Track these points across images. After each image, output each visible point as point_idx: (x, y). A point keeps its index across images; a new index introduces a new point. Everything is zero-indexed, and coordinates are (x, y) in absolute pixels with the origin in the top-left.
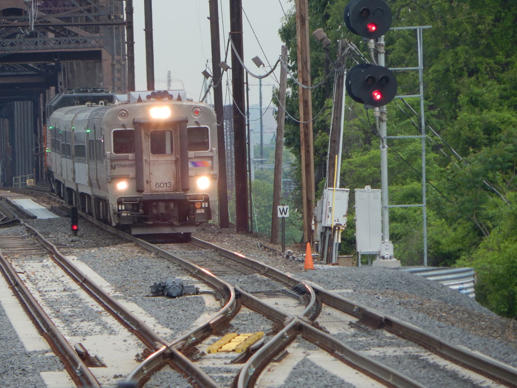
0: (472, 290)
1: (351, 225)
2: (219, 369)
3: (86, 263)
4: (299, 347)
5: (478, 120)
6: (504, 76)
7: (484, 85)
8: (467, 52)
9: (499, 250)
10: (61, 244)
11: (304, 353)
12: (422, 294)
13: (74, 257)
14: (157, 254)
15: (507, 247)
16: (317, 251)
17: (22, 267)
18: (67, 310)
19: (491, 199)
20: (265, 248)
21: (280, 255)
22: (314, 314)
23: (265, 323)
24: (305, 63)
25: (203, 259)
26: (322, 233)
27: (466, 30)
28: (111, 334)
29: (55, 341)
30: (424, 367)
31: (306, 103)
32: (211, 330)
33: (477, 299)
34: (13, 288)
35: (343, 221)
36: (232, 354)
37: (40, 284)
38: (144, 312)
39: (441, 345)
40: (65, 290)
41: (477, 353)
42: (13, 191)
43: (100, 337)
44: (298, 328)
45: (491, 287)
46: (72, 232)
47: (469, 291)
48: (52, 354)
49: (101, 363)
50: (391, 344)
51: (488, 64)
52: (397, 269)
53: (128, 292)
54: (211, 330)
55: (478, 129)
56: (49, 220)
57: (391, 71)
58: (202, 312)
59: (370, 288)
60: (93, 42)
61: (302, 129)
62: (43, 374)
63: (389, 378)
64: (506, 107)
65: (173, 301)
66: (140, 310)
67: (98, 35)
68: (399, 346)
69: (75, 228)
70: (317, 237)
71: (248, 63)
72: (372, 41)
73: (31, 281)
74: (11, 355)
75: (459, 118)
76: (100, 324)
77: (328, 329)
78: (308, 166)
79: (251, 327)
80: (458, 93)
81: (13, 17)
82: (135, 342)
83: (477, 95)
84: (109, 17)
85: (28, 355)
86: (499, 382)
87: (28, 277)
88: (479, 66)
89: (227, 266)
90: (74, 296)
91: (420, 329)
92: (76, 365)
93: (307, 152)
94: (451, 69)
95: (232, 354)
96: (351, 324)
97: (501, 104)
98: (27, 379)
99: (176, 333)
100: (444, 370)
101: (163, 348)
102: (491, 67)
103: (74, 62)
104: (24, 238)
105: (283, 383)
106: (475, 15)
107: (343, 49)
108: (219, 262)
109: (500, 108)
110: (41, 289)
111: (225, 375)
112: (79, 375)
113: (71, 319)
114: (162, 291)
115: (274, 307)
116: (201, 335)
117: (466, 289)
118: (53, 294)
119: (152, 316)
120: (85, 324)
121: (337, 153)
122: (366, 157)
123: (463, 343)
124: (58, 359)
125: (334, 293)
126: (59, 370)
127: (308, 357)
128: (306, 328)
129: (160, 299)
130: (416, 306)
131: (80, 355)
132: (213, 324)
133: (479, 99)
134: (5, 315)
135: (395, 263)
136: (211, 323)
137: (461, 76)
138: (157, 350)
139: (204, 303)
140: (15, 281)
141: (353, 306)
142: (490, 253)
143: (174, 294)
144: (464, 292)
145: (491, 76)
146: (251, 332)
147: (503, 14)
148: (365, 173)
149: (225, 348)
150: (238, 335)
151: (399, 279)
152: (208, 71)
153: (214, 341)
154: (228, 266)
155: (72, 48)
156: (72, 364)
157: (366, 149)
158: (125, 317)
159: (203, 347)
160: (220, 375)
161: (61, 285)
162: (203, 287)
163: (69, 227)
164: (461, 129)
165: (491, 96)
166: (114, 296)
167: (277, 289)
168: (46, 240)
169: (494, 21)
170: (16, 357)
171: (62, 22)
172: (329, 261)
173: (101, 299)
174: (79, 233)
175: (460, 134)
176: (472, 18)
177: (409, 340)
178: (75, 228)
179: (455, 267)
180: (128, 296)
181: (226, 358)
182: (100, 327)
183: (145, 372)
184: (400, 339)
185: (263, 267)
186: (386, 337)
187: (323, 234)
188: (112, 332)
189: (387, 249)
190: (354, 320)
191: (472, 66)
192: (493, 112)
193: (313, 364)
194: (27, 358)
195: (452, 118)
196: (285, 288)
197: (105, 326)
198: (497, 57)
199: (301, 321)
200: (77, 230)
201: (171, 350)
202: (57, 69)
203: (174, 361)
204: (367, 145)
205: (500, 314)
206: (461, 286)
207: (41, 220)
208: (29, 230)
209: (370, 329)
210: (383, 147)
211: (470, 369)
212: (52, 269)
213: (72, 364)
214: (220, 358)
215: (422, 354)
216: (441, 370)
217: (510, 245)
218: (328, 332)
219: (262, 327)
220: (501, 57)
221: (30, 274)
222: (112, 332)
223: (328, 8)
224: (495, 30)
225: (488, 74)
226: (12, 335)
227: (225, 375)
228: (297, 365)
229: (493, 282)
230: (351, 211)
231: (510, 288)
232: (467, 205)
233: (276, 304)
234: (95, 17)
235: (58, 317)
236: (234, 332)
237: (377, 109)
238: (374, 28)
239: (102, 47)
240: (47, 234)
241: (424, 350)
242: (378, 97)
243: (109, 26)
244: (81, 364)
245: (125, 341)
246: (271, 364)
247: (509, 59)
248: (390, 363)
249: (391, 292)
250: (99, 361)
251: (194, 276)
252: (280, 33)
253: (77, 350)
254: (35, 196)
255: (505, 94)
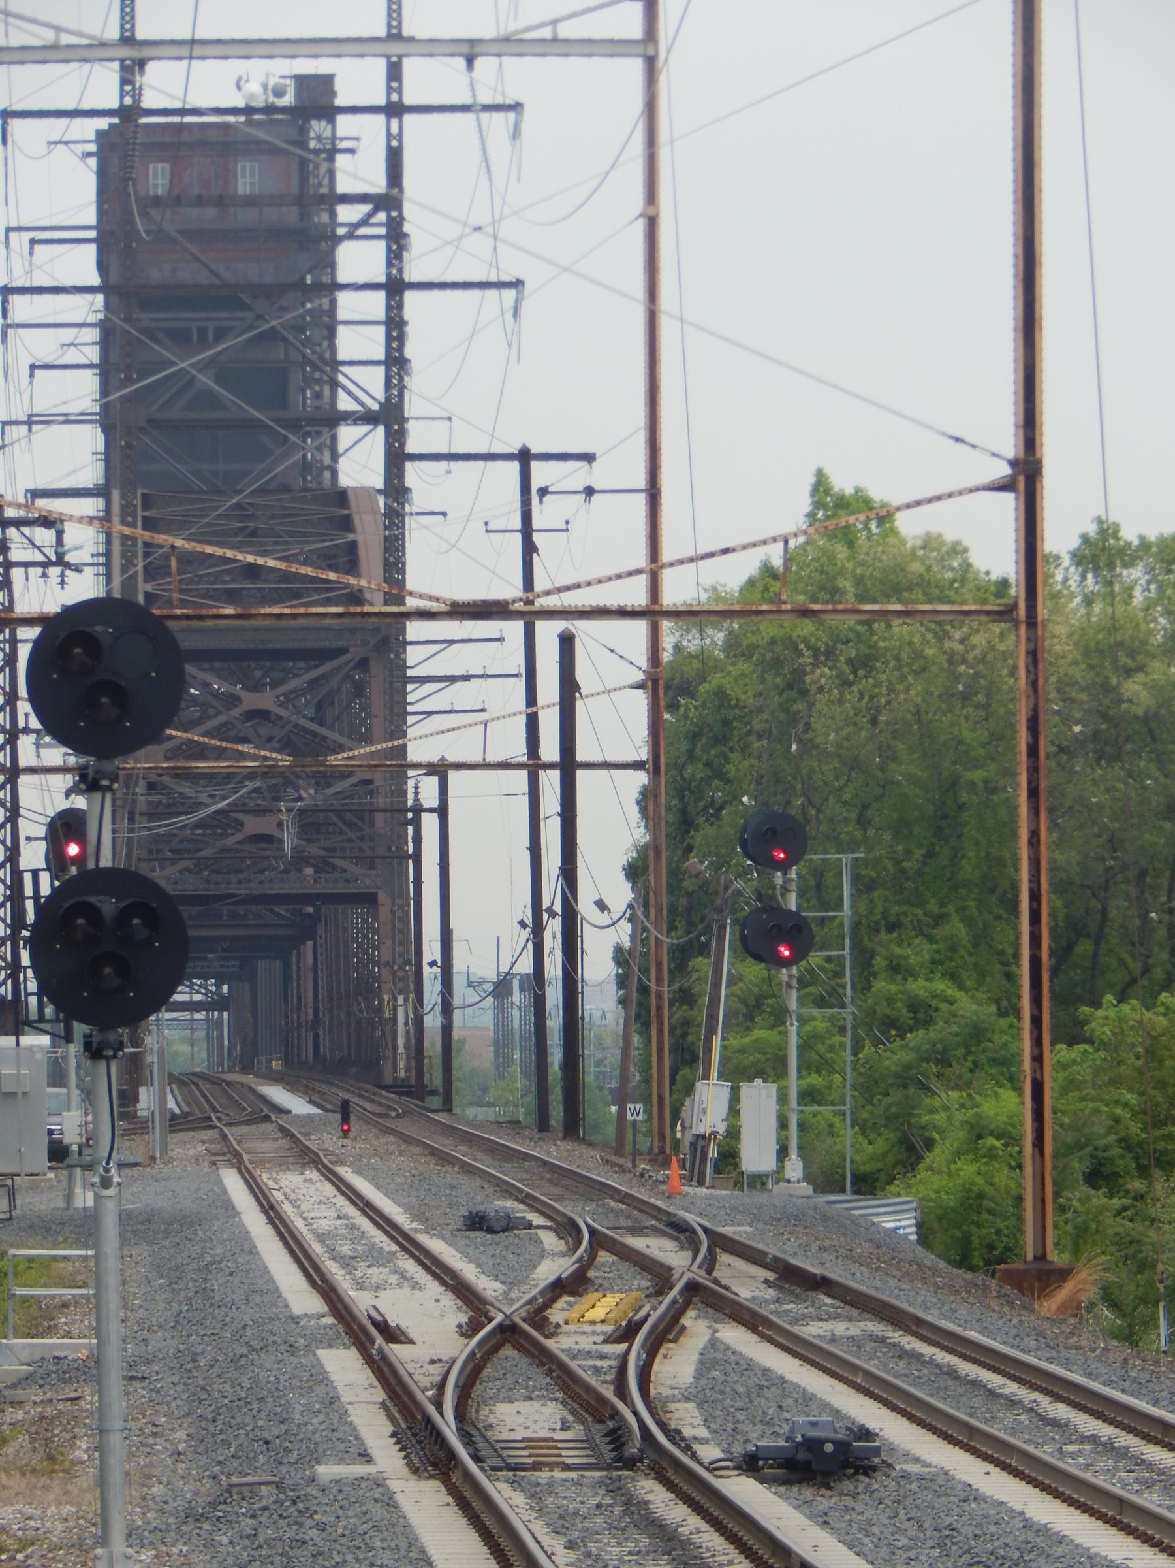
0: (914, 1229)
1: (734, 1133)
2: (589, 1352)
3: (365, 1178)
4: (698, 1317)
5: (900, 992)
6: (937, 932)
7: (909, 945)
8: (886, 899)
9: (950, 1174)
10: (327, 1150)
11: (709, 1327)
12: (845, 1235)
13: (346, 1169)
14: (462, 1167)
15: (960, 1170)
16: (684, 1168)
17: (276, 1181)
18: (346, 1247)
19: (928, 1101)
20: (607, 1161)
21: (630, 1172)
22: (710, 1265)
23: (639, 1277)
24: (659, 910)
25: (528, 1176)
26: (692, 1144)
27: (885, 868)
28: (413, 1288)
29: (335, 1299)
30: (900, 1357)
31: (659, 965)
32: (564, 1287)
33: (919, 1241)
34: (266, 1212)
35: (721, 1128)
36: (600, 1328)
37: (304, 1207)
38: (458, 1255)
39: (919, 1321)
40: (339, 1217)
41: (973, 1335)
42: (257, 1076)
43: (398, 1292)
44: (693, 1288)
45: (936, 1226)
46: (341, 1134)
47: (909, 1230)
48: (329, 1320)
49: (407, 1337)
50: (837, 1317)
51: (915, 915)
52: (808, 1197)
53: (430, 1222)
54: (564, 1287)
55: (899, 1004)
56: (309, 1116)
57: (804, 919)
58: (542, 1256)
59: (771, 1225)
60: (368, 882)
61: (653, 1001)
62: (320, 1352)
63: (857, 1376)
64: (939, 975)
65: (496, 1237)
66: (451, 1251)
67: (373, 872)
68: (850, 1320)
69: (346, 1127)
70: (686, 1147)
71: (585, 906)
72: (779, 874)
73: (291, 1202)
74: (270, 1318)
75: (873, 989)
76: (396, 1272)
77: (734, 1289)
78: (660, 1050)
79: (620, 1282)
80: (873, 955)
81: (263, 845)
82: (452, 1303)
83: (900, 957)
84: (389, 849)
85: (295, 1320)
86: (1030, 1387)
87: (286, 1195)
88: (903, 918)
89: (563, 1187)
90: (353, 1227)
91: (872, 1292)
92: (373, 1342)
93: (660, 1031)
94: (864, 921)
95: (600, 1328)
96: (766, 1281)
97: (932, 972)
98: (295, 1361)
99: (510, 1290)
100: (931, 1362)
101: (499, 1318)
102: (919, 921)
103: (340, 907)
104: (277, 1139)
105: (691, 1380)
106: (900, 848)
107: (726, 888)
108: (551, 1181)
109: (931, 976)
110: (305, 1215)
111: (599, 1363)
112: (377, 1358)
113: (354, 1263)
114: (480, 1223)
115: (647, 1251)
116: (549, 1295)
117: (904, 1227)
118: (323, 1223)
119: (470, 1262)
120: (374, 1271)
121: (716, 1033)
122: (747, 1040)
123: (944, 1316)
124: (341, 1328)
125: (727, 1230)
126: (346, 1347)
127: (717, 1335)
128: (706, 1288)
129: (478, 1236)
130: (842, 1251)
131: (375, 1323)
132: (567, 1278)
133: (903, 963)
134: (258, 1253)
135: (806, 1188)
136: (564, 1276)
137: (878, 931)
138: (490, 1320)
139: (542, 1242)
140: (268, 1201)
141: (765, 1254)
142: (936, 1178)
143: (497, 1228)
144: (902, 1231)
145: (921, 933)
146: (620, 1291)
147: (937, 848)
148: (746, 1062)
149: (589, 1316)
150: (604, 1296)
151: (811, 1212)
152: (525, 919)
153: (570, 1304)
154: (566, 1187)
155: (340, 889)
156: (363, 1338)
157: (748, 1029)
158: (432, 1263)
159: (556, 1314)
160: (591, 1363)
161: (333, 1209)
162: (538, 1220)
163: (336, 1125)
164: (877, 1004)
165: (919, 959)
166: (411, 1229)
167: (642, 1225)
168: (307, 1143)
169: (924, 856)
170: (277, 1322)
171: (323, 853)
172: (701, 1183)
173: (393, 1233)
174: (351, 1134)
175: (874, 1012)
176: (895, 852)
177: (863, 1310)
178: (346, 1127)
179: (886, 1197)
180: (431, 1228)
181: (594, 1333)
182: (397, 1276)
183: (478, 1356)
184: (848, 1308)
185: (618, 1191)
186: (826, 1305)
187: (693, 1145)
188: (415, 1286)
189: (793, 1170)
190: (771, 1276)
191: (892, 919)
192: (921, 982)
193: (728, 1348)
194: (294, 1326)
195: (863, 989)
196: (653, 1222)
197: (403, 1275)
198: (928, 906)
199: (697, 1278)
200: (349, 1130)
201: (511, 1320)
202: (316, 918)
203: (516, 1336)
204: (749, 1023)
205: (951, 1263)
206: (898, 1224)
207: (298, 1116)
208: (282, 1129)
209: (798, 1290)
210: (792, 1025)
211: (974, 1363)
212: (318, 1185)
213: (363, 1338)
214: (584, 1333)
215: (890, 1334)
216: (925, 1361)
217: (965, 1167)
218: (737, 1294)
219: (636, 1283)
220: (933, 907)
221: (288, 1191)
222: (415, 1286)
223: (692, 837)
224: (926, 869)
225: (914, 929)
226: (270, 1286)
227: (599, 1363)
228: (704, 1349)
229: (940, 1219)
230: (734, 1110)
231: (965, 1227)
232: (894, 1109)
233: (648, 1246)
234: (370, 847)
235: (334, 1259)
236: (596, 1290)
237: (784, 970)
238: (782, 855)
239: (378, 888)
240: (307, 1135)
241: (890, 1328)
242: (787, 953)
243: (389, 860)
244: (379, 1340)
245: (437, 1301)
246: (666, 1345)
247: (944, 910)
248: (845, 1348)
249: (800, 1229)
250: (403, 1333)
251: (521, 1202)
252: (624, 869)
253: (369, 1315)
254: (288, 1083)
255: (937, 957)
